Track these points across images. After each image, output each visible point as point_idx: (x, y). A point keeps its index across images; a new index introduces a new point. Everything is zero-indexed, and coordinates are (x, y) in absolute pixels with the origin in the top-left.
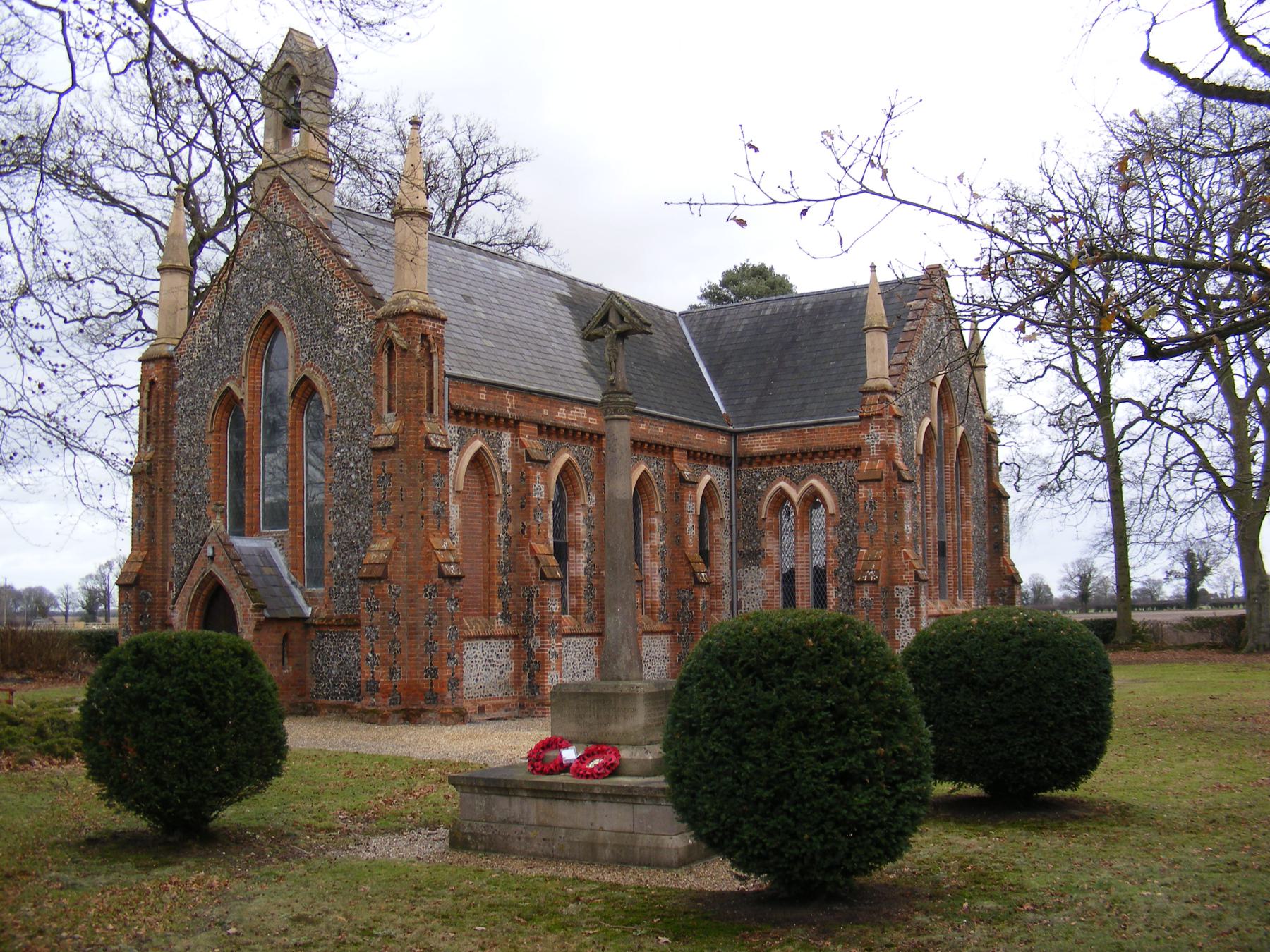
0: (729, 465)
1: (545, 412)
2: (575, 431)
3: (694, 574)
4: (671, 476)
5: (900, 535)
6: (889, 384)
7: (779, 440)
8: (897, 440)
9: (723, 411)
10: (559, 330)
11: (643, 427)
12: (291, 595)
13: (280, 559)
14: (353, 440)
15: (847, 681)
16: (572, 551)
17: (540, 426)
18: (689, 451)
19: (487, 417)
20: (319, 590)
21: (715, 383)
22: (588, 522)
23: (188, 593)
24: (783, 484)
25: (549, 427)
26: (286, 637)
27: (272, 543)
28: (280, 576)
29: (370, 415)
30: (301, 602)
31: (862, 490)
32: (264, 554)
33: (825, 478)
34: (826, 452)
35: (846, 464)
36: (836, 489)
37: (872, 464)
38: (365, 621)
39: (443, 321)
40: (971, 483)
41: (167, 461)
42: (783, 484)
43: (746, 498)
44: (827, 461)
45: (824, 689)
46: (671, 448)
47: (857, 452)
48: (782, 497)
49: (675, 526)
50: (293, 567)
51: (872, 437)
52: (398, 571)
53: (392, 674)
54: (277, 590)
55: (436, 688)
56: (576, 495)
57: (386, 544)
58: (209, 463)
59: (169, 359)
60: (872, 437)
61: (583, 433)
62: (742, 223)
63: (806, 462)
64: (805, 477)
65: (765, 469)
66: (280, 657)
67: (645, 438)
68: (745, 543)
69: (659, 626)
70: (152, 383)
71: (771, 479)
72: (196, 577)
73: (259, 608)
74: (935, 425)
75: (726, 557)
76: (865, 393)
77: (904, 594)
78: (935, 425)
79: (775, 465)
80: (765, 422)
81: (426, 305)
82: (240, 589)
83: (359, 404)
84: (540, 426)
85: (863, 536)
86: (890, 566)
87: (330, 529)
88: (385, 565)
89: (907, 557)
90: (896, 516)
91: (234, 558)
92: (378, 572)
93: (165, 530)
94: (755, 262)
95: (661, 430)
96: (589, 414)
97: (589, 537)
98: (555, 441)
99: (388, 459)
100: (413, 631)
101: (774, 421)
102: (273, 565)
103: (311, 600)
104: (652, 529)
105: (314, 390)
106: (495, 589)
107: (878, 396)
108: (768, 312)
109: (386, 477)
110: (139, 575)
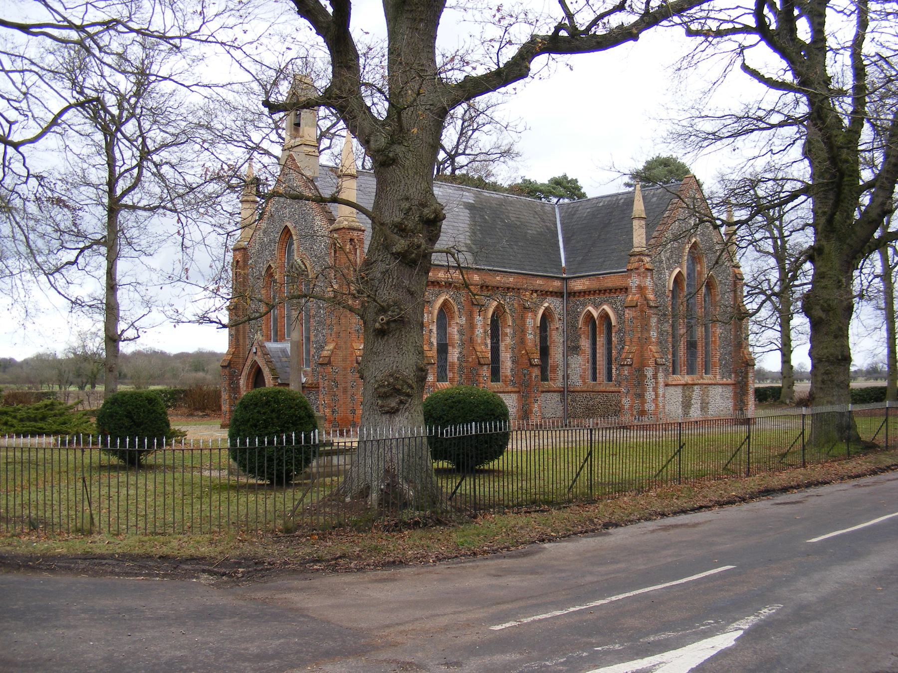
0: (563, 297)
5: (648, 338)
7: (587, 283)
8: (648, 282)
9: (563, 265)
10: (456, 224)
11: (498, 278)
15: (273, 411)
16: (450, 348)
21: (564, 248)
22: (461, 332)
23: (246, 371)
24: (590, 308)
31: (627, 311)
33: (611, 304)
36: (615, 310)
37: (633, 297)
38: (321, 385)
39: (363, 231)
42: (590, 308)
43: (571, 315)
44: (612, 295)
45: (264, 413)
47: (625, 290)
48: (589, 315)
49: (520, 331)
51: (634, 282)
55: (355, 420)
56: (453, 318)
59: (245, 249)
60: (634, 282)
63: (602, 296)
64: (601, 304)
69: (509, 389)
70: (238, 262)
72: (249, 363)
73: (275, 379)
74: (685, 272)
75: (560, 350)
76: (631, 256)
77: (649, 372)
78: (685, 272)
80: (582, 272)
81: (353, 224)
82: (267, 369)
85: (627, 339)
86: (642, 356)
87: (313, 339)
88: (330, 357)
89: (651, 351)
90: (646, 327)
93: (244, 338)
95: (511, 279)
97: (461, 340)
100: (345, 391)
101: (586, 271)
104: (506, 334)
107: (638, 257)
108: (601, 204)
110: (230, 361)
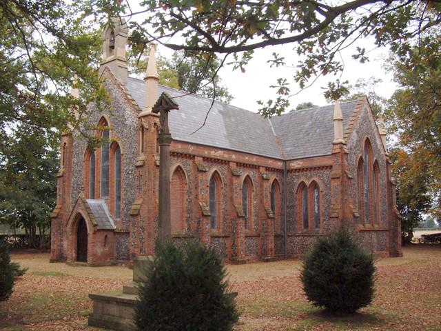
0: (283, 173)
1: (206, 152)
2: (218, 160)
3: (267, 214)
4: (259, 177)
6: (344, 142)
12: (109, 221)
13: (106, 207)
14: (131, 163)
17: (204, 158)
18: (237, 163)
19: (181, 154)
20: (118, 219)
25: (207, 158)
26: (106, 236)
27: (104, 201)
28: (105, 214)
29: (136, 155)
30: (113, 224)
32: (100, 206)
34: (319, 168)
35: (327, 172)
40: (379, 179)
41: (70, 172)
46: (259, 167)
48: (303, 184)
50: (111, 211)
52: (144, 213)
53: (141, 251)
54: (104, 219)
57: (140, 202)
58: (83, 172)
61: (222, 161)
62: (322, 88)
64: (312, 177)
65: (297, 174)
66: (103, 244)
67: (247, 163)
68: (289, 203)
71: (298, 178)
72: (74, 214)
79: (301, 173)
83: (133, 150)
84: (204, 158)
91: (87, 208)
92: (136, 213)
94: (307, 102)
96: (224, 153)
98: (210, 164)
99: (141, 169)
102: (103, 210)
103: (116, 222)
105: (118, 146)
106: (185, 219)
109: (140, 177)
